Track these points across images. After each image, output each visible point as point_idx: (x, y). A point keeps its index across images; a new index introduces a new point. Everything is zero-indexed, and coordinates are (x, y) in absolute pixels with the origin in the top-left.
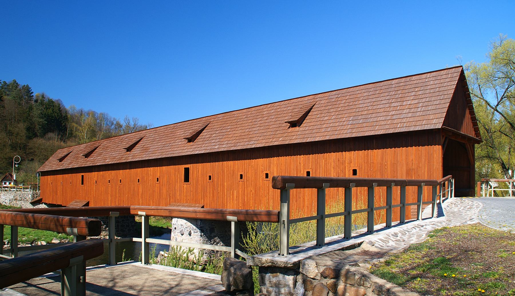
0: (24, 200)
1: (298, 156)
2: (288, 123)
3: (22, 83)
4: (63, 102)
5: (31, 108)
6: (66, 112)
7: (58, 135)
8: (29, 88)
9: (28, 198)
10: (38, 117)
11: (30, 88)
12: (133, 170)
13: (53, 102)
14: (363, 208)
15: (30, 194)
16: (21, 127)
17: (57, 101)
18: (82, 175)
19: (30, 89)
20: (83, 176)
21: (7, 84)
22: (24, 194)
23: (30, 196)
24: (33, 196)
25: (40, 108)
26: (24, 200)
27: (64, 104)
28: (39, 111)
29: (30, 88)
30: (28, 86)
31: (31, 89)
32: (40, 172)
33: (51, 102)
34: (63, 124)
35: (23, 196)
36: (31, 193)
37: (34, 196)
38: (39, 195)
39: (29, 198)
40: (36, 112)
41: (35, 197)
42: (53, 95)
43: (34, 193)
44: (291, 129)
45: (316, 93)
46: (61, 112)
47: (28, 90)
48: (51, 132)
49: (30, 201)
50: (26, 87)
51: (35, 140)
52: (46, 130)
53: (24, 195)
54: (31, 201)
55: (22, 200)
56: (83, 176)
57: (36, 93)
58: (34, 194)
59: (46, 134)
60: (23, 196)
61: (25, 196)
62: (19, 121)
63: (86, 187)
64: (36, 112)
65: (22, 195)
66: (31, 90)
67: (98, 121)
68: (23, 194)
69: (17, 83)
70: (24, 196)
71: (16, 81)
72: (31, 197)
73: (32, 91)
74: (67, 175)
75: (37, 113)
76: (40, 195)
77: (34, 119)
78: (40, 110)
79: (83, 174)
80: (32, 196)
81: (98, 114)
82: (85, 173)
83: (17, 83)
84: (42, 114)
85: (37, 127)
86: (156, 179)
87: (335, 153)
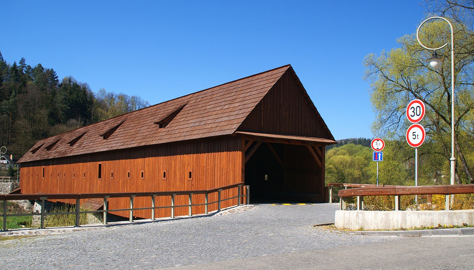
0: (4, 191)
1: (239, 151)
2: (156, 124)
3: (46, 66)
4: (90, 85)
5: (54, 94)
6: (92, 96)
7: (81, 121)
8: (53, 72)
9: (8, 189)
10: (61, 102)
11: (55, 72)
12: (72, 165)
13: (78, 86)
14: (163, 208)
15: (10, 185)
16: (44, 112)
17: (84, 84)
18: (99, 164)
19: (54, 73)
20: (100, 165)
21: (31, 68)
22: (4, 184)
23: (10, 187)
24: (13, 188)
25: (64, 93)
26: (4, 191)
27: (91, 88)
28: (63, 97)
29: (55, 72)
30: (52, 70)
31: (56, 73)
32: (20, 163)
33: (76, 86)
34: (89, 109)
35: (3, 187)
36: (11, 183)
37: (14, 187)
38: (19, 185)
39: (9, 189)
40: (60, 97)
41: (15, 188)
42: (80, 79)
43: (14, 184)
44: (160, 129)
45: (168, 100)
46: (86, 97)
47: (51, 73)
48: (73, 118)
49: (10, 192)
50: (50, 72)
51: (57, 126)
52: (70, 115)
53: (4, 186)
54: (11, 191)
55: (2, 191)
56: (100, 165)
57: (61, 77)
58: (14, 185)
59: (68, 120)
60: (3, 187)
61: (5, 187)
62: (41, 107)
63: (45, 179)
64: (60, 97)
65: (2, 186)
66: (56, 74)
67: (129, 105)
68: (3, 185)
69: (43, 67)
70: (4, 187)
71: (42, 65)
72: (10, 188)
73: (57, 75)
74: (35, 167)
75: (61, 98)
76: (19, 186)
77: (57, 105)
78: (63, 95)
79: (100, 163)
80: (11, 186)
81: (130, 97)
82: (45, 166)
83: (42, 68)
84: (66, 100)
85: (61, 112)
86: (128, 173)
87: (206, 153)
